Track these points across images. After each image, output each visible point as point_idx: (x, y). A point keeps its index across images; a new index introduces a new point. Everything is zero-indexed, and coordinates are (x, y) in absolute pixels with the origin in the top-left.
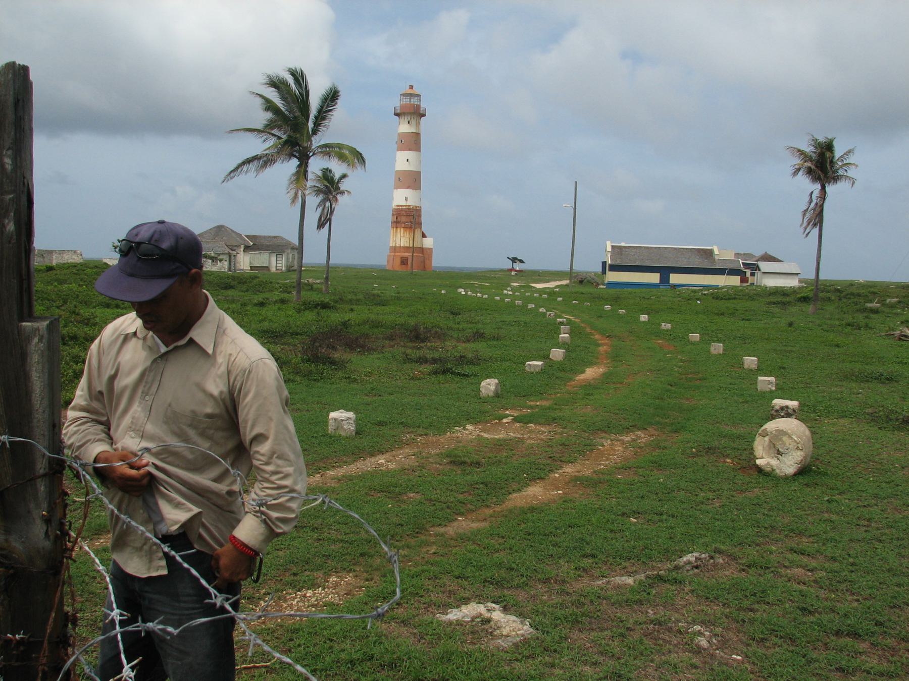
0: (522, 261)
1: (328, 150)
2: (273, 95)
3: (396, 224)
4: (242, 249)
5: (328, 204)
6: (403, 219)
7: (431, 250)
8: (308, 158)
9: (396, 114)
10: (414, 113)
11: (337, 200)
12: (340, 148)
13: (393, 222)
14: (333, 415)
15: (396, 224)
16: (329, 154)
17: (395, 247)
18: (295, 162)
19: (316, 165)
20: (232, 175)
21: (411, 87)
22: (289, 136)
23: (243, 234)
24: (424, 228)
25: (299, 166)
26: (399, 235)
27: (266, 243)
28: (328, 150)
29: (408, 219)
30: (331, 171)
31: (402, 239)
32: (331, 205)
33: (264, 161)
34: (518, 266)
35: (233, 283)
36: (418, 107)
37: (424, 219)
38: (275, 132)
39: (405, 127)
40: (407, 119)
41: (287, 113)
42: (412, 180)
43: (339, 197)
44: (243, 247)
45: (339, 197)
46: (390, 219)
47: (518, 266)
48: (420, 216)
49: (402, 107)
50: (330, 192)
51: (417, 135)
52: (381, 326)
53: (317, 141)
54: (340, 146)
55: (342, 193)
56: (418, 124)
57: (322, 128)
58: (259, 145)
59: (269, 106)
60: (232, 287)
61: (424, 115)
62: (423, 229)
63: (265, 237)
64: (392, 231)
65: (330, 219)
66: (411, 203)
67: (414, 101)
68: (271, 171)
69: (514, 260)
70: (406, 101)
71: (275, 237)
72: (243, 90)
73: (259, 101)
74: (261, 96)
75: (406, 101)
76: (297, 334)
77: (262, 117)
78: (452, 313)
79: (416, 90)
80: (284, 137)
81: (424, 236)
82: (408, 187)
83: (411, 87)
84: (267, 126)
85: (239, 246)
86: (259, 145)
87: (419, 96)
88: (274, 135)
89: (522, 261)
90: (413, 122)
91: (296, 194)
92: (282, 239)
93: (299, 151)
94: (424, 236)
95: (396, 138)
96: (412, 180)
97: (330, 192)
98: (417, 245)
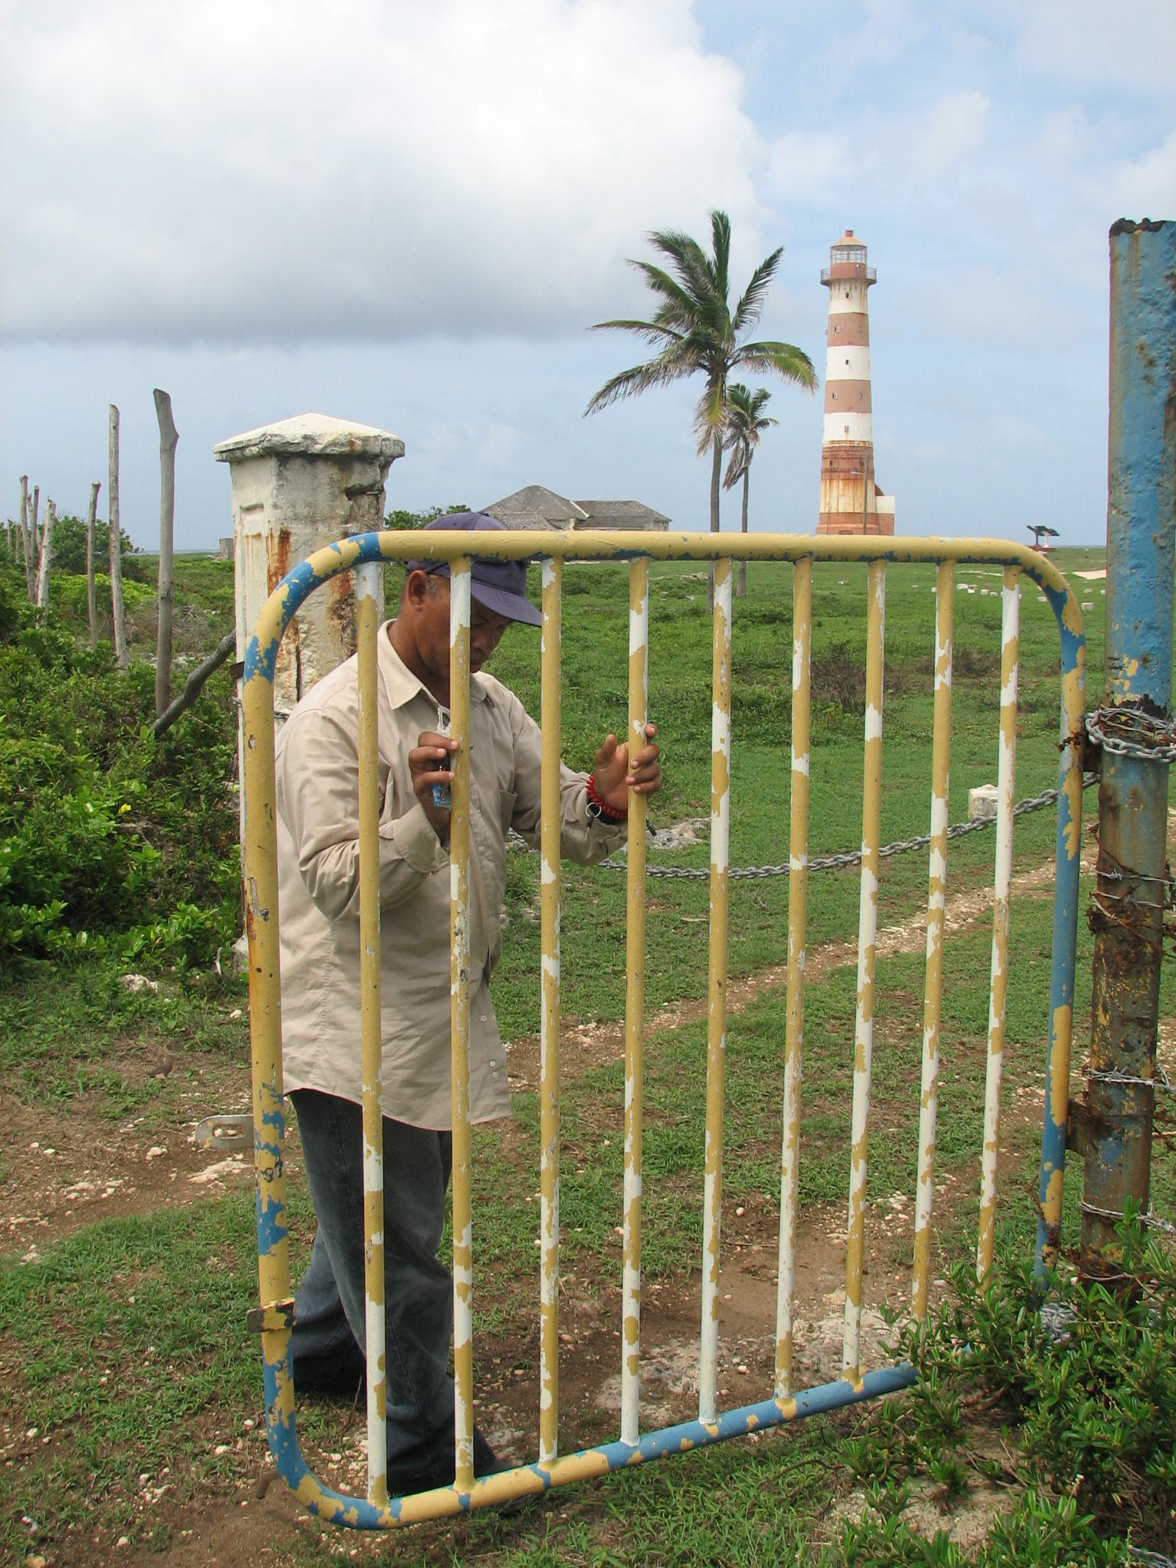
0: (1053, 533)
1: (758, 353)
2: (667, 265)
3: (830, 473)
4: (572, 525)
5: (742, 445)
6: (843, 465)
7: (891, 516)
8: (726, 369)
9: (826, 283)
10: (859, 279)
11: (756, 437)
12: (776, 352)
13: (825, 471)
14: (976, 793)
15: (830, 473)
16: (761, 362)
17: (829, 514)
18: (702, 377)
19: (736, 376)
20: (601, 401)
21: (850, 233)
22: (694, 334)
23: (573, 498)
24: (879, 480)
25: (710, 383)
26: (835, 492)
27: (611, 513)
28: (758, 353)
29: (851, 464)
30: (743, 389)
31: (841, 499)
32: (747, 445)
33: (640, 376)
34: (1046, 541)
35: (584, 583)
36: (863, 267)
37: (878, 464)
38: (673, 327)
39: (840, 304)
40: (844, 289)
41: (688, 293)
42: (857, 396)
43: (760, 431)
44: (572, 522)
45: (760, 431)
46: (818, 464)
47: (1046, 541)
48: (871, 458)
49: (834, 269)
50: (745, 424)
51: (863, 316)
52: (897, 651)
53: (743, 338)
54: (777, 347)
55: (763, 423)
56: (863, 297)
57: (748, 317)
58: (647, 350)
59: (659, 281)
60: (583, 591)
61: (873, 282)
62: (876, 482)
63: (609, 503)
64: (822, 487)
65: (745, 469)
66: (856, 436)
67: (855, 258)
68: (655, 392)
69: (1040, 531)
70: (841, 258)
71: (626, 503)
72: (610, 259)
73: (644, 274)
74: (644, 266)
75: (841, 258)
76: (769, 666)
77: (651, 303)
78: (987, 626)
79: (858, 239)
80: (686, 336)
81: (878, 493)
82: (850, 409)
83: (850, 233)
84: (659, 317)
85: (566, 521)
86: (647, 350)
87: (863, 248)
88: (670, 333)
89: (1053, 533)
90: (855, 294)
91: (708, 433)
92: (640, 506)
93: (711, 359)
94: (878, 493)
95: (826, 325)
96: (857, 396)
97: (745, 424)
98: (870, 510)
